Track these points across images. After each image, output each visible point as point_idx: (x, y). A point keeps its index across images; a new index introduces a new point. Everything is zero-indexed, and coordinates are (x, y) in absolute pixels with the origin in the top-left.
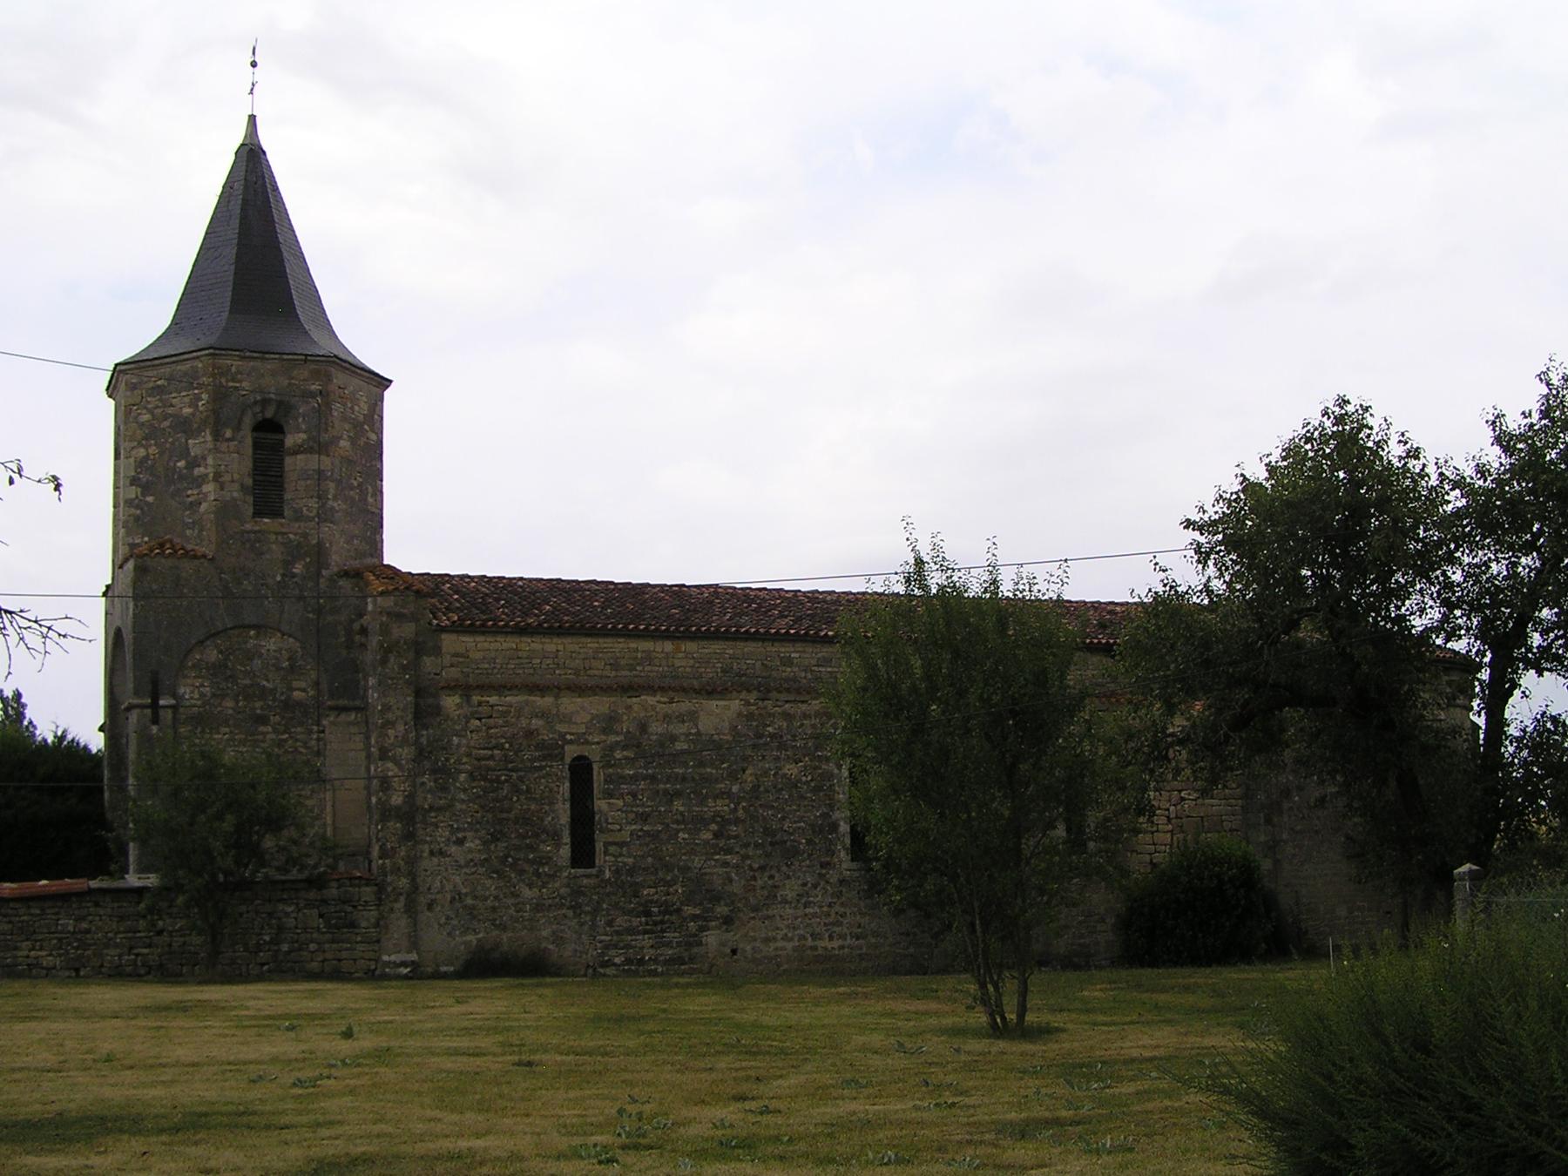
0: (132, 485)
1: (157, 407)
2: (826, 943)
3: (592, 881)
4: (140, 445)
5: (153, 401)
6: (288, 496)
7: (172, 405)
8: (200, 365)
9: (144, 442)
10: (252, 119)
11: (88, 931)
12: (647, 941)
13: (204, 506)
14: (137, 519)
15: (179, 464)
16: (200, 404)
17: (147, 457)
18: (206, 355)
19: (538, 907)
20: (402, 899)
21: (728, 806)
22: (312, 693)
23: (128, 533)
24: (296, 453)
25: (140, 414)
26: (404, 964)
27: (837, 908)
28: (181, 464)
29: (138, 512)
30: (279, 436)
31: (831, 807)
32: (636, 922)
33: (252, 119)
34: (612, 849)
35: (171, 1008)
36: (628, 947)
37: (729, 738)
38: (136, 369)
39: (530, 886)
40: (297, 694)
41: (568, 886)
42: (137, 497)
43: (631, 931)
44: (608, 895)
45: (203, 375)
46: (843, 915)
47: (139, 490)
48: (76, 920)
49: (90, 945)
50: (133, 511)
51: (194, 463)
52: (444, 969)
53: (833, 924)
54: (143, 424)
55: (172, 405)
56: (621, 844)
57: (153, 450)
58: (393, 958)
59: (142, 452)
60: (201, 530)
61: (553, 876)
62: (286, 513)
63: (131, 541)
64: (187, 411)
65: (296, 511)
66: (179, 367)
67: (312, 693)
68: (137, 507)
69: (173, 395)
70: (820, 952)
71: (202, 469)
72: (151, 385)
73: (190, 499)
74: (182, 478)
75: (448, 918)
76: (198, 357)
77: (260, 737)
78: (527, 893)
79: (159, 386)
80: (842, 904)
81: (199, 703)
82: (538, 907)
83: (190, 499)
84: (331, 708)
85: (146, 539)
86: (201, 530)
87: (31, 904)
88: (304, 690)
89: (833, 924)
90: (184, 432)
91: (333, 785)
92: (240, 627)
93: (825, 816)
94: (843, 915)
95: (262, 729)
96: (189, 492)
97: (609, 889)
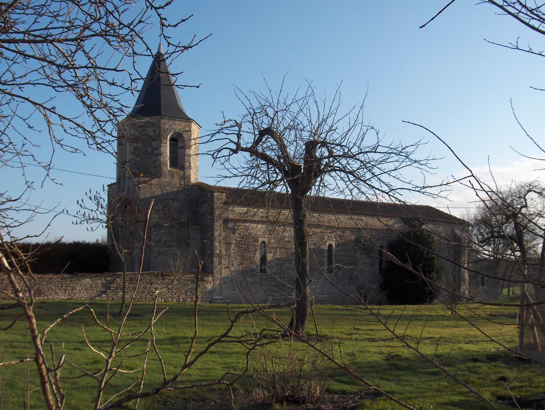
1: (141, 132)
2: (320, 296)
3: (265, 277)
6: (179, 161)
12: (278, 294)
17: (138, 146)
19: (252, 284)
20: (219, 280)
22: (186, 219)
26: (219, 299)
27: (324, 286)
28: (150, 149)
31: (323, 257)
32: (275, 289)
34: (270, 268)
36: (273, 296)
39: (250, 278)
40: (182, 220)
41: (259, 278)
43: (274, 291)
44: (269, 281)
46: (325, 288)
52: (228, 301)
53: (323, 291)
56: (272, 267)
58: (216, 297)
61: (256, 275)
62: (178, 166)
67: (186, 219)
70: (319, 298)
75: (229, 286)
78: (249, 280)
80: (325, 285)
82: (252, 284)
84: (191, 224)
88: (184, 219)
89: (323, 291)
91: (522, 214)
92: (168, 199)
93: (322, 260)
94: (325, 288)
95: (173, 230)
97: (269, 279)
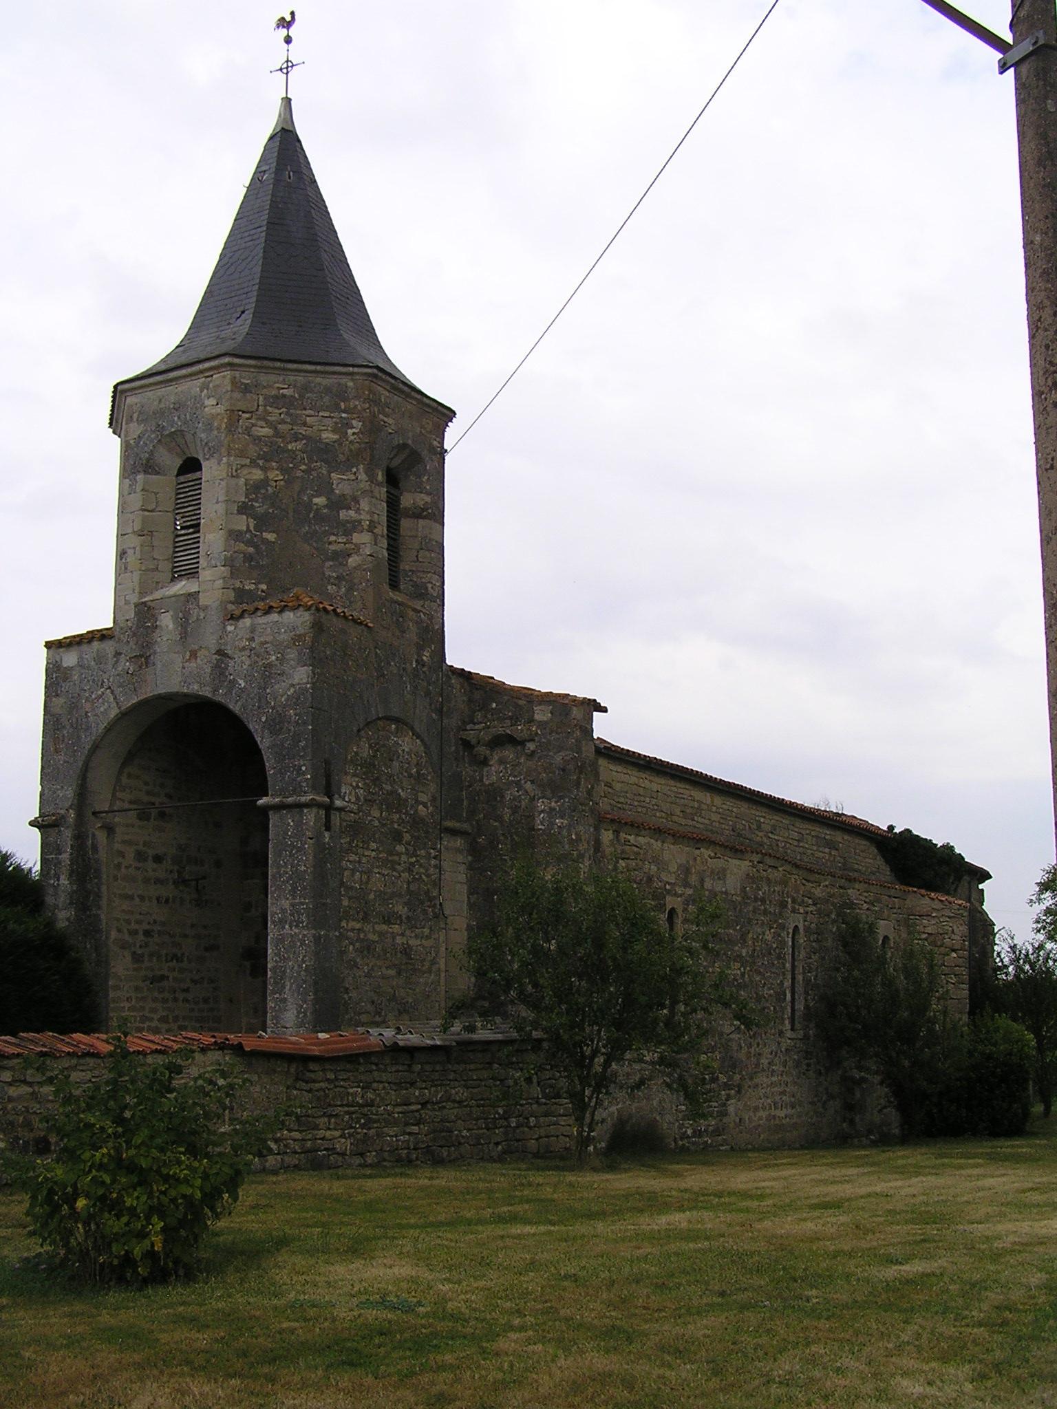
0: (240, 512)
1: (283, 422)
4: (254, 463)
5: (275, 414)
7: (305, 424)
8: (351, 384)
9: (261, 462)
10: (287, 101)
11: (371, 1104)
13: (353, 561)
14: (248, 558)
15: (316, 500)
16: (350, 431)
17: (265, 483)
18: (365, 374)
21: (739, 969)
23: (233, 575)
24: (418, 516)
25: (253, 425)
28: (320, 501)
29: (251, 550)
30: (197, 475)
33: (287, 101)
35: (814, 1207)
37: (739, 899)
38: (255, 367)
42: (248, 530)
45: (355, 397)
47: (252, 523)
48: (363, 1088)
49: (375, 1122)
50: (242, 546)
51: (338, 503)
54: (259, 438)
55: (305, 424)
57: (275, 475)
59: (257, 475)
60: (350, 589)
63: (238, 585)
64: (328, 436)
65: (415, 585)
66: (318, 380)
68: (249, 543)
69: (308, 412)
71: (352, 513)
72: (274, 392)
73: (332, 547)
74: (319, 518)
76: (352, 374)
77: (396, 858)
79: (284, 396)
81: (355, 807)
83: (332, 547)
85: (264, 587)
86: (350, 589)
87: (327, 1066)
90: (326, 461)
96: (333, 538)
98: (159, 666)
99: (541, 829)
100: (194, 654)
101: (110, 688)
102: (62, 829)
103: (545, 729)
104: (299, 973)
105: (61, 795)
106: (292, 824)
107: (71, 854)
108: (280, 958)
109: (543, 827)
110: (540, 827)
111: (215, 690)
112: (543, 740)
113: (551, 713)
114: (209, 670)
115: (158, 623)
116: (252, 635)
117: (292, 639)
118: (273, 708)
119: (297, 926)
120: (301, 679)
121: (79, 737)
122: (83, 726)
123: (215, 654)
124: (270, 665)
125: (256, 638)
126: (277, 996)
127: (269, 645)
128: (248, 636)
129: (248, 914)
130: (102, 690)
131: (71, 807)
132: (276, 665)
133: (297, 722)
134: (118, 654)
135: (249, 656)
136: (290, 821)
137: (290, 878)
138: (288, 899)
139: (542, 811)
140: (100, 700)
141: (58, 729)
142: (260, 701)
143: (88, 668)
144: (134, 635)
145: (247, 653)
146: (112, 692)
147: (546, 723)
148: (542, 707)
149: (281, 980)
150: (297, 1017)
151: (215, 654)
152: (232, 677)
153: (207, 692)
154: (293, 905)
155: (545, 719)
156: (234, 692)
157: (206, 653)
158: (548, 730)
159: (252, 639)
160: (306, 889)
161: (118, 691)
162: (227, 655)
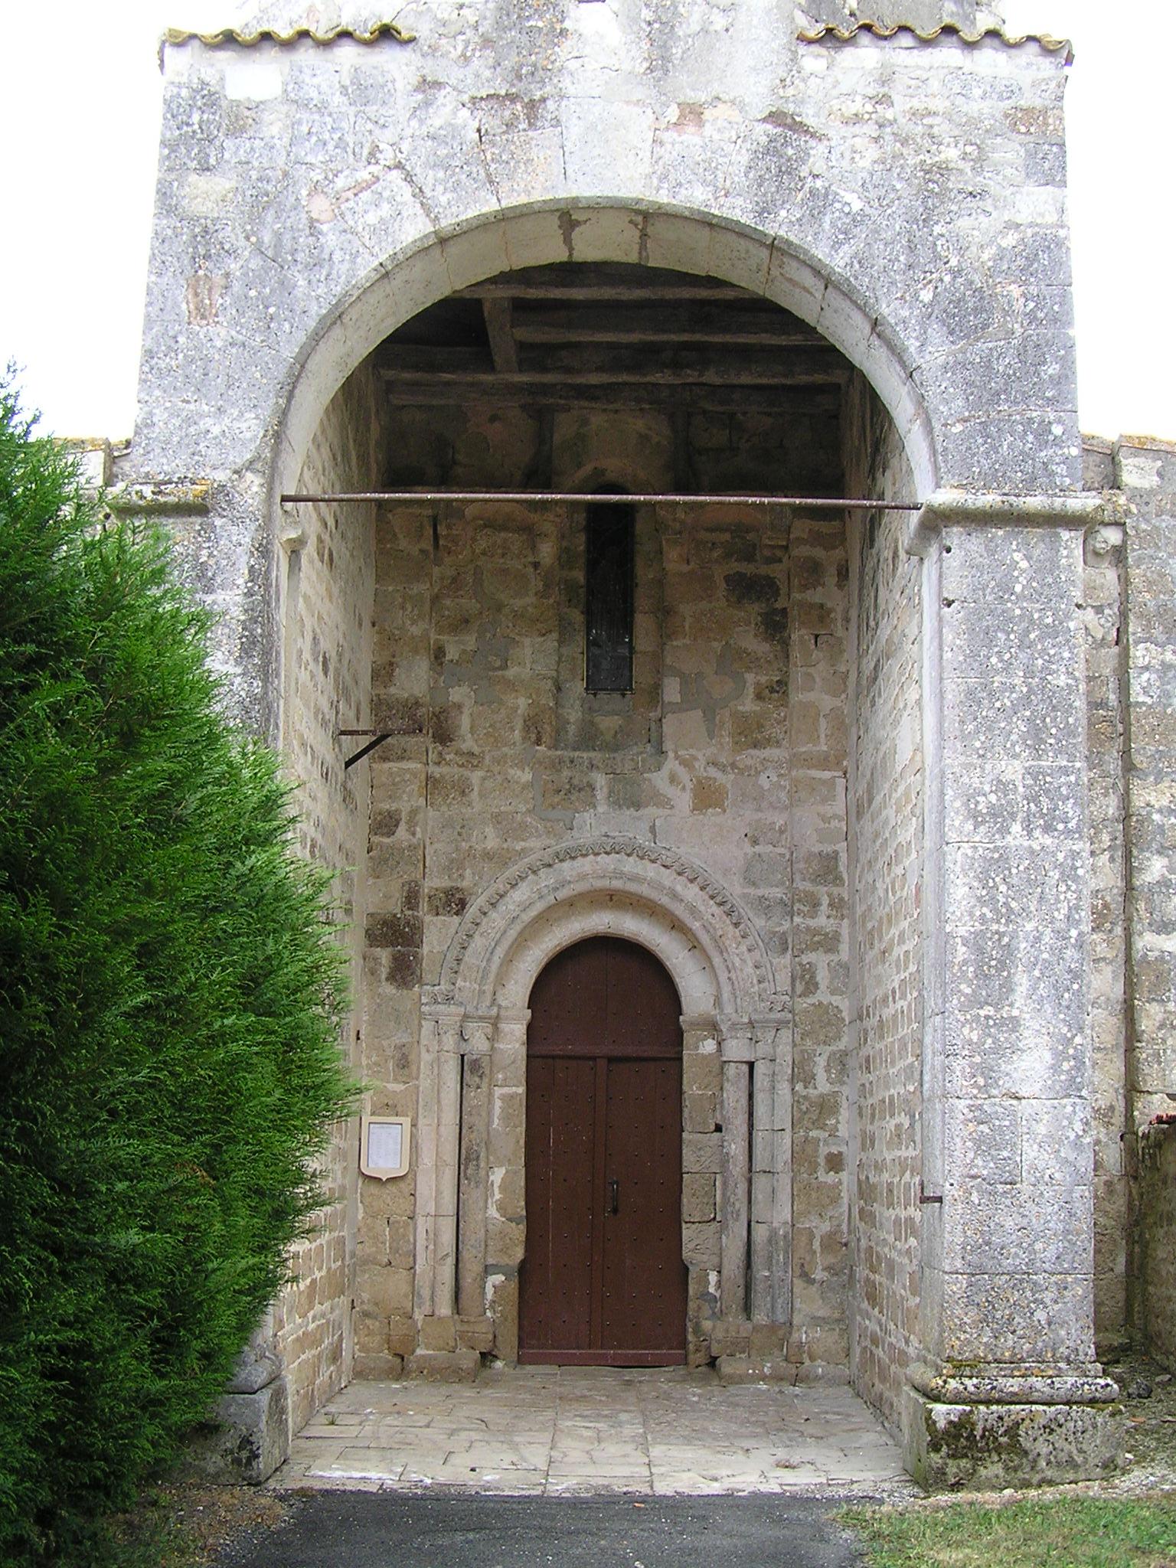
98: (574, 130)
99: (1144, 703)
100: (692, 113)
101: (399, 166)
102: (218, 522)
103: (1147, 504)
104: (1059, 954)
105: (216, 431)
106: (1024, 564)
107: (249, 594)
108: (993, 910)
109: (1149, 701)
110: (1140, 699)
111: (762, 212)
112: (1143, 526)
113: (1160, 474)
114: (744, 158)
115: (567, 24)
116: (883, 90)
117: (1007, 116)
118: (956, 273)
119: (1048, 829)
120: (1042, 215)
121: (285, 286)
122: (300, 256)
123: (764, 120)
124: (943, 169)
125: (895, 98)
126: (988, 1010)
127: (937, 120)
128: (871, 92)
129: (386, 840)
130: (372, 168)
131: (250, 466)
132: (961, 171)
133: (1031, 317)
134: (428, 86)
135: (876, 140)
136: (1017, 556)
137: (1026, 700)
138: (1016, 756)
139: (1146, 668)
140: (366, 196)
141: (207, 257)
142: (911, 248)
143: (322, 108)
144: (487, 42)
145: (871, 129)
146: (409, 178)
147: (1152, 492)
148: (1140, 461)
149: (999, 970)
150: (1055, 1068)
151: (764, 120)
152: (819, 183)
153: (738, 210)
154: (1034, 774)
155: (1147, 486)
156: (827, 219)
157: (735, 116)
158: (1152, 508)
159: (885, 100)
160: (1072, 734)
161: (428, 178)
162: (798, 127)
